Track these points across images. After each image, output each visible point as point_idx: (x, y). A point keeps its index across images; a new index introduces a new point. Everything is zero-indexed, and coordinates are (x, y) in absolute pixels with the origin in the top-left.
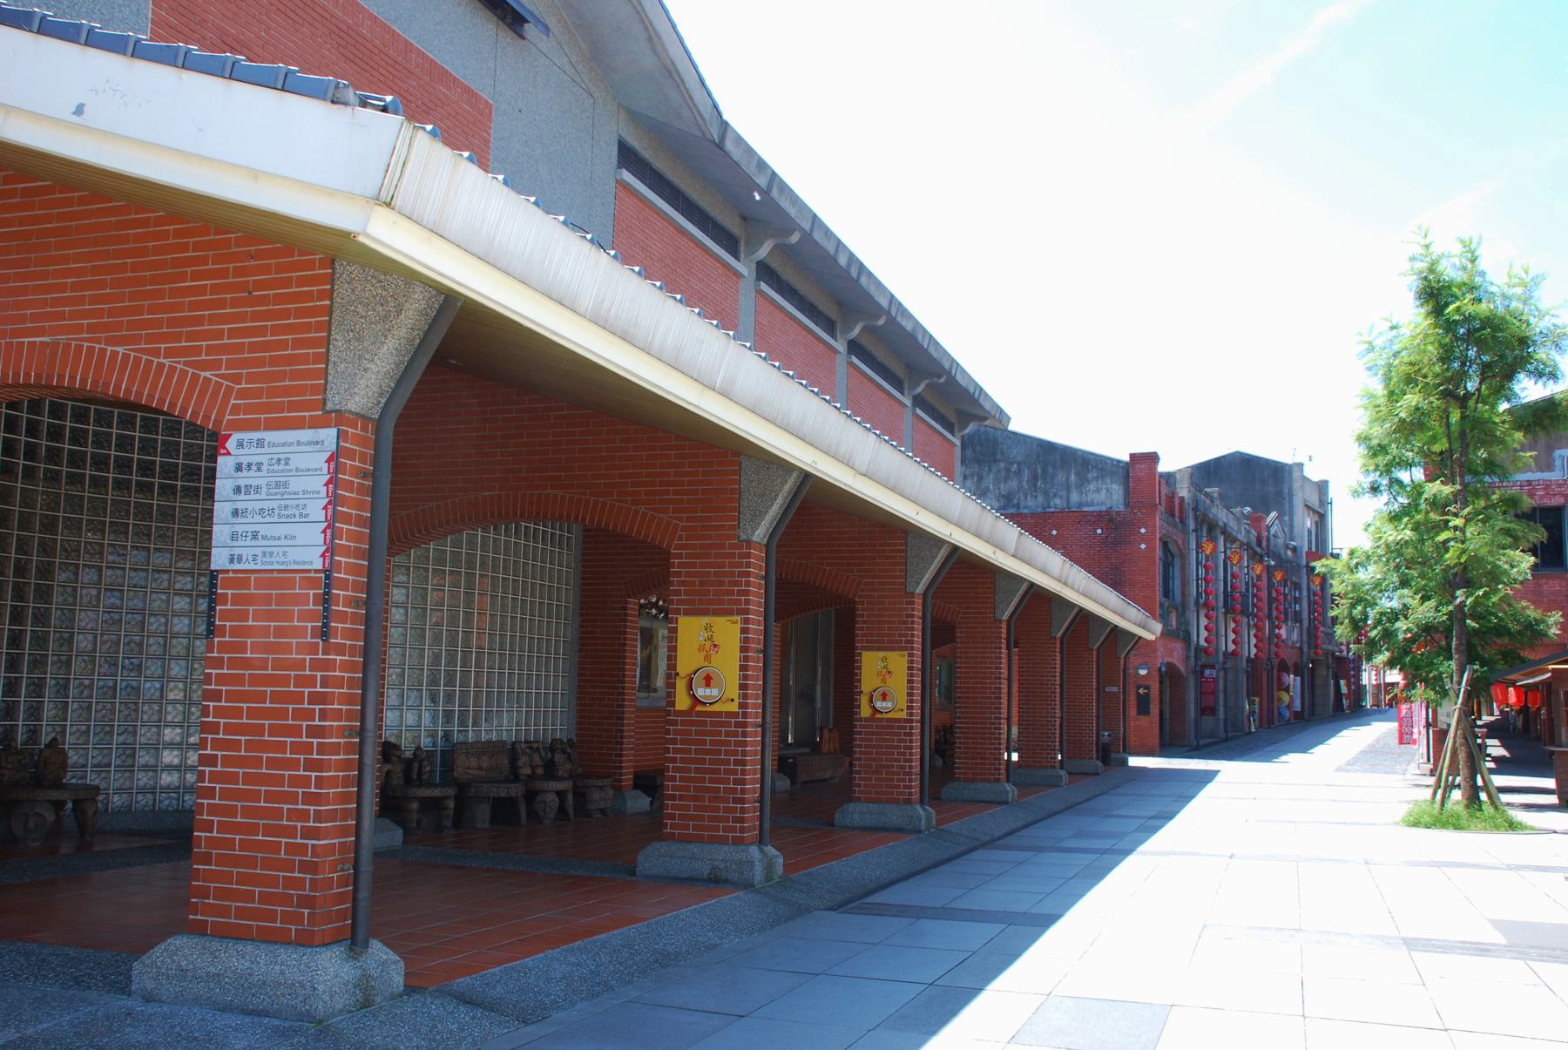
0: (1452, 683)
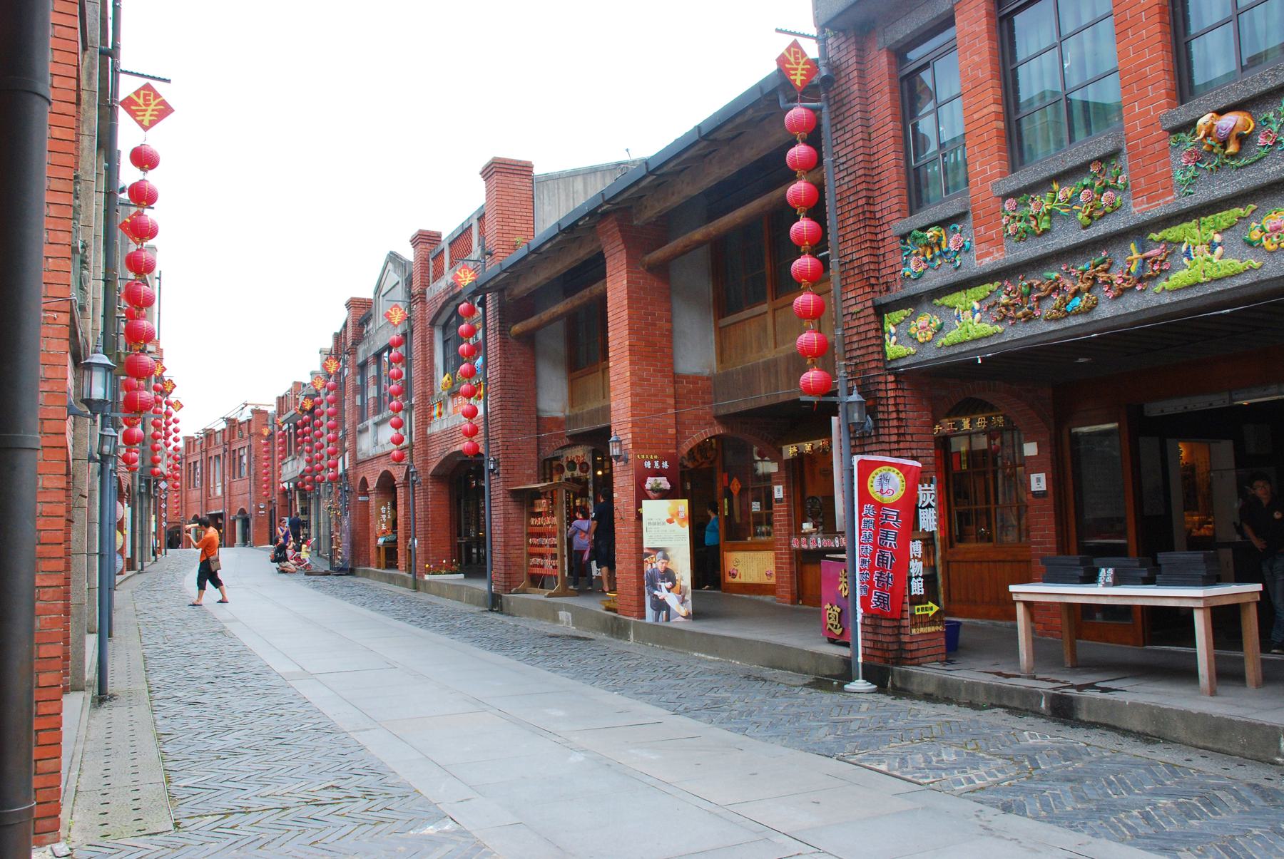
0: (973, 318)
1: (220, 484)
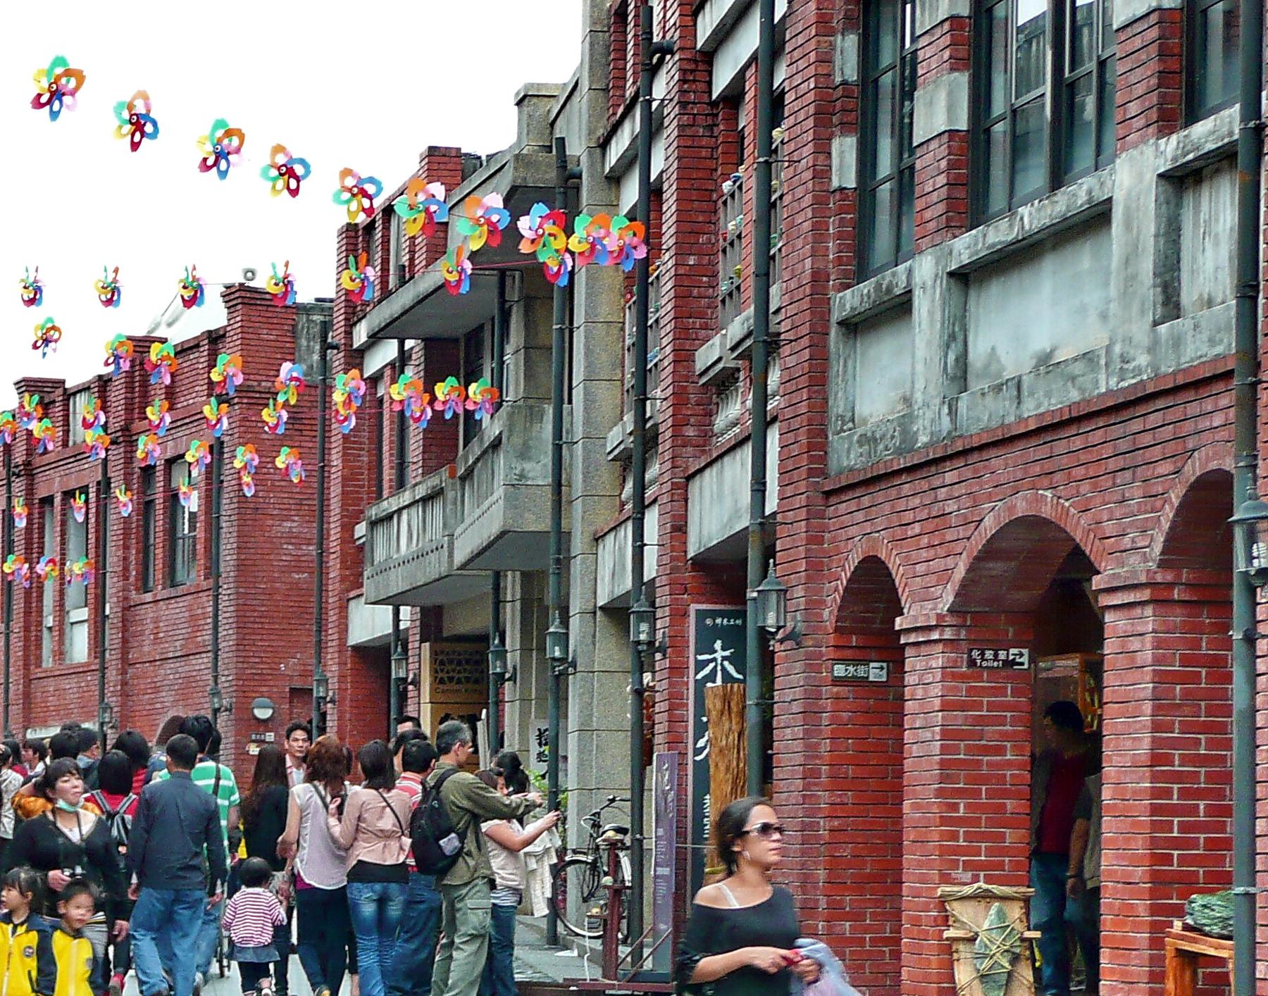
1: (83, 614)
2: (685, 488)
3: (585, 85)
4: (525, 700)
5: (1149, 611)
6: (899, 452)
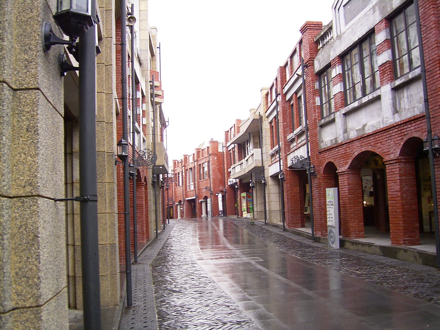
1: (193, 183)
2: (287, 157)
3: (262, 105)
4: (256, 190)
5: (397, 164)
6: (347, 140)
